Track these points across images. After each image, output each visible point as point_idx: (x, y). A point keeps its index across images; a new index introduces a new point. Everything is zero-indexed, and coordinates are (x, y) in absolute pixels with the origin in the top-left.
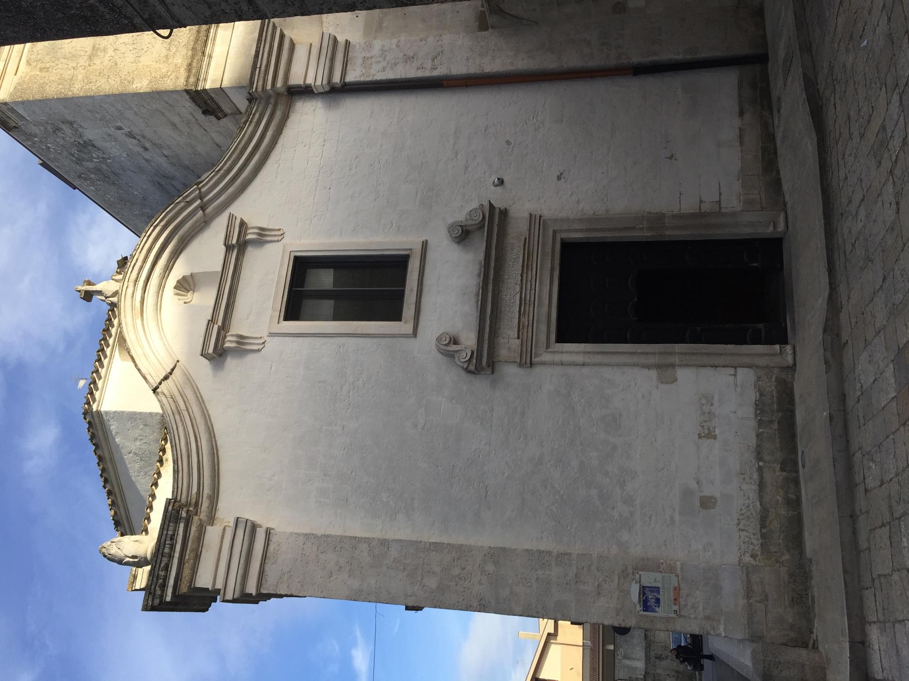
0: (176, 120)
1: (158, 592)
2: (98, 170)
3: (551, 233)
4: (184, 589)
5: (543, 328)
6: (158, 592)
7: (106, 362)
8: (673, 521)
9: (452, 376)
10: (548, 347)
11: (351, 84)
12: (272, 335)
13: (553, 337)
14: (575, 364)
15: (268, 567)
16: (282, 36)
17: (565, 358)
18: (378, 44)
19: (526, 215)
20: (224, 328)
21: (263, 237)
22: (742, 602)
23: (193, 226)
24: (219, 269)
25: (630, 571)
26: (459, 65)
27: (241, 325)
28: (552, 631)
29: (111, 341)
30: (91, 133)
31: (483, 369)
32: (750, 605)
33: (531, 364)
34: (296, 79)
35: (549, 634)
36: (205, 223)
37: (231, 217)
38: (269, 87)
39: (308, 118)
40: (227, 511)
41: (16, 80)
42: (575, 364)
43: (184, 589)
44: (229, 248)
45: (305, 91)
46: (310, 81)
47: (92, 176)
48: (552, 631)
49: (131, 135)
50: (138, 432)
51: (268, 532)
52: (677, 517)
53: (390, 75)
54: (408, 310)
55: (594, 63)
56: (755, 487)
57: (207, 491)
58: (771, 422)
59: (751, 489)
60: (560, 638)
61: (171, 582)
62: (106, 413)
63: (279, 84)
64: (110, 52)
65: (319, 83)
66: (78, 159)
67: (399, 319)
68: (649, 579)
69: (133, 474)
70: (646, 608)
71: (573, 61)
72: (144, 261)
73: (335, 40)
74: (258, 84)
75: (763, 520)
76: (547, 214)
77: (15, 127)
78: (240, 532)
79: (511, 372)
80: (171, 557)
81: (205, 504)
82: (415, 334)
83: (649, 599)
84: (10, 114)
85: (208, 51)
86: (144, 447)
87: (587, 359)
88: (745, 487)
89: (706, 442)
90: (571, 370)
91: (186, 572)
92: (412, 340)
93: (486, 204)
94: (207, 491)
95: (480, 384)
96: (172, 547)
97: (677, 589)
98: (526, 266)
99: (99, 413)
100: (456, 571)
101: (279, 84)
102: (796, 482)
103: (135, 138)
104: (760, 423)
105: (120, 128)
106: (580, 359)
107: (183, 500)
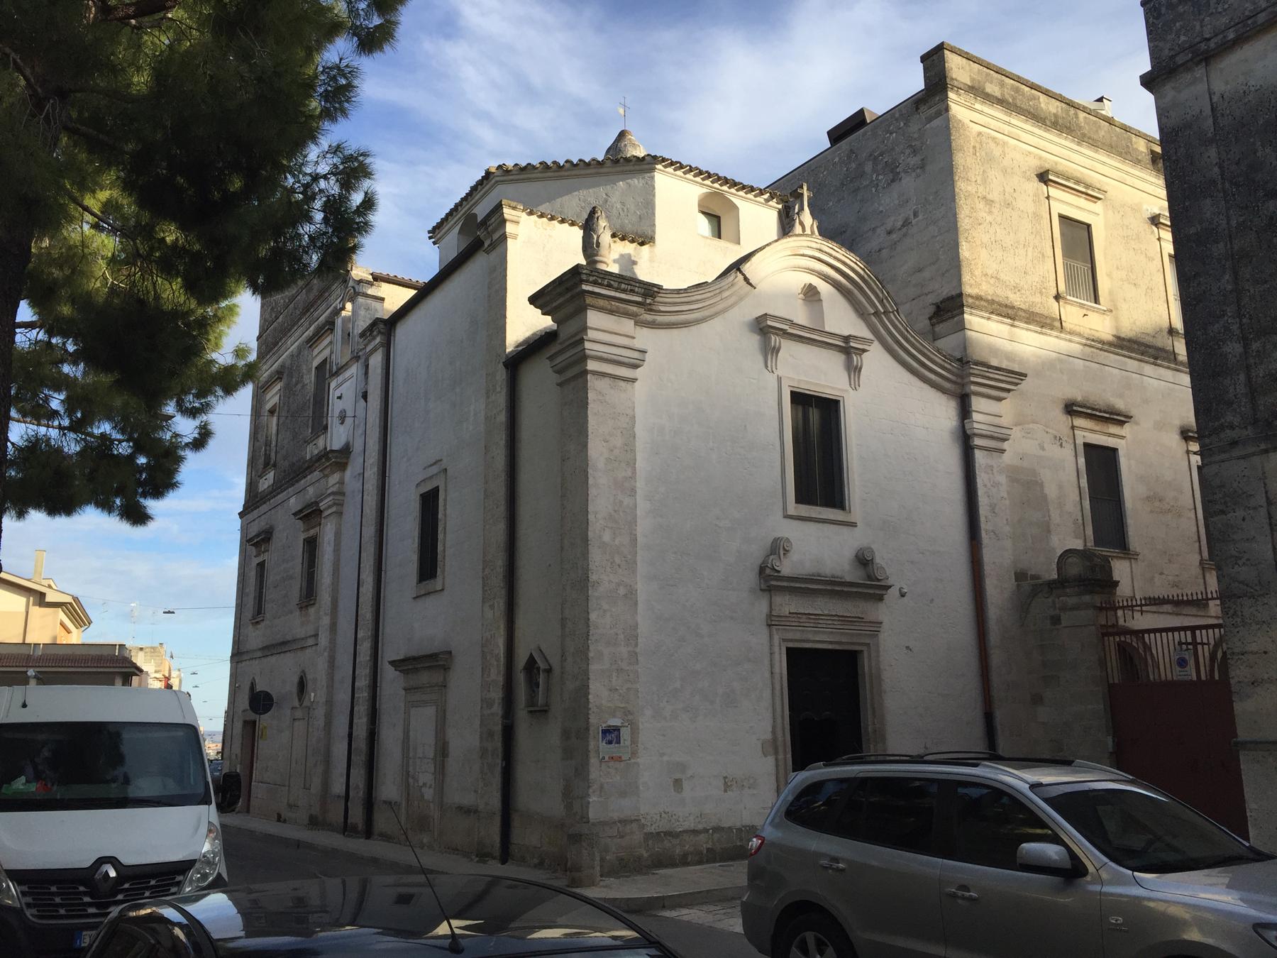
0: (927, 274)
1: (591, 279)
2: (862, 175)
3: (867, 641)
4: (589, 300)
5: (798, 636)
6: (591, 279)
7: (698, 179)
8: (662, 755)
9: (756, 552)
10: (784, 640)
11: (973, 454)
12: (779, 379)
13: (791, 645)
14: (772, 666)
15: (607, 380)
16: (1009, 391)
17: (777, 656)
18: (1002, 479)
19: (880, 619)
20: (785, 334)
21: (854, 370)
22: (616, 816)
23: (861, 302)
24: (827, 329)
25: (630, 717)
26: (991, 555)
27: (789, 350)
28: (48, 599)
29: (716, 185)
30: (908, 183)
31: (766, 581)
32: (615, 823)
33: (769, 626)
34: (978, 404)
35: (43, 595)
36: (861, 313)
37: (870, 342)
38: (972, 379)
39: (943, 412)
40: (644, 338)
41: (967, 121)
42: (772, 666)
43: (589, 300)
44: (846, 339)
45: (965, 411)
46: (975, 416)
47: (854, 165)
48: (48, 599)
49: (906, 223)
50: (632, 208)
51: (634, 380)
52: (665, 758)
53: (981, 492)
54: (805, 510)
55: (995, 679)
56: (692, 826)
57: (660, 319)
58: (741, 840)
59: (690, 824)
60: (36, 611)
61: (597, 290)
62: (653, 178)
63: (973, 388)
64: (989, 218)
65: (975, 425)
66: (876, 158)
67: (798, 501)
68: (625, 733)
69: (583, 193)
70: (605, 732)
71: (996, 658)
72: (836, 258)
73: (1005, 440)
74: (977, 369)
75: (669, 834)
76: (882, 636)
77: (917, 109)
78: (636, 355)
79: (762, 607)
80: (616, 290)
81: (649, 317)
82: (787, 516)
83: (611, 734)
84: (933, 110)
85: (993, 316)
86: (614, 211)
87: (777, 677)
88: (691, 818)
89: (721, 783)
90: (767, 662)
91: (601, 302)
92: (781, 513)
93: (890, 582)
94: (660, 319)
95: (751, 578)
96: (624, 291)
97: (619, 759)
98: (844, 619)
99: (654, 169)
100: (617, 560)
101: (973, 388)
102: (700, 862)
103: (903, 226)
104: (739, 830)
105: (916, 215)
106: (777, 670)
107: (658, 299)
